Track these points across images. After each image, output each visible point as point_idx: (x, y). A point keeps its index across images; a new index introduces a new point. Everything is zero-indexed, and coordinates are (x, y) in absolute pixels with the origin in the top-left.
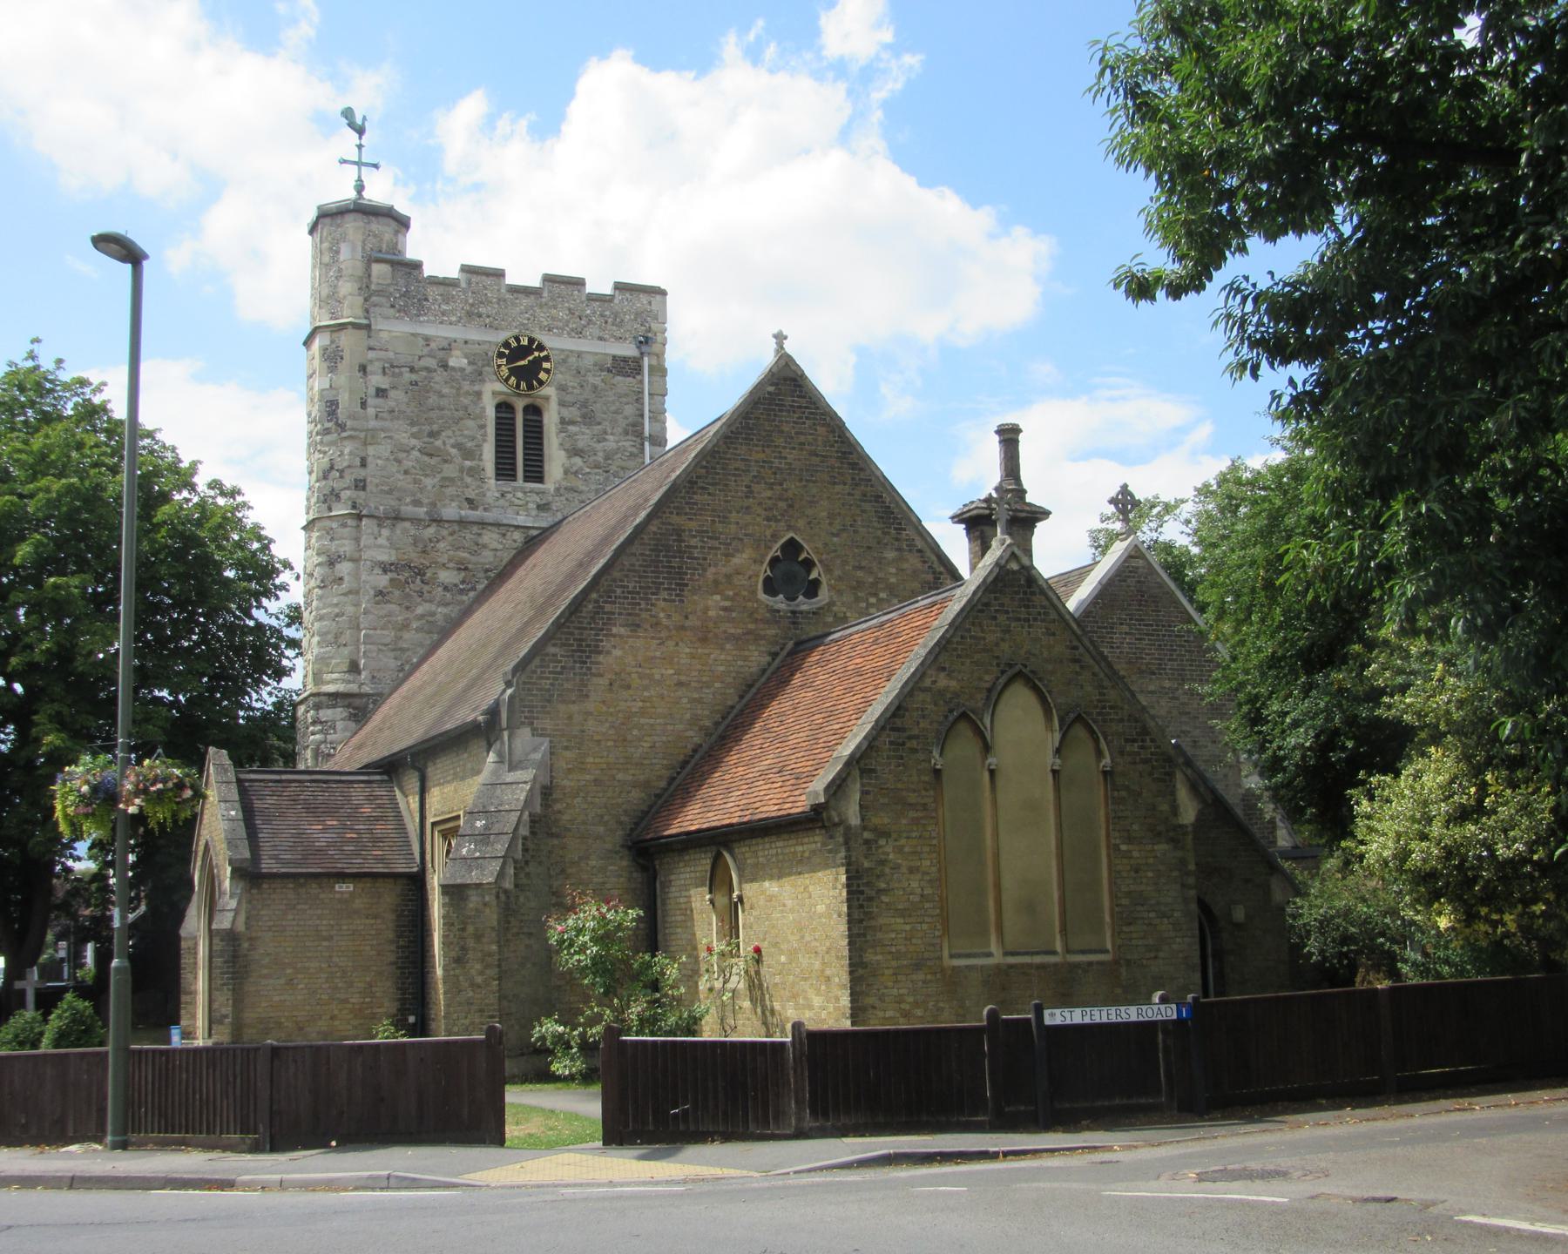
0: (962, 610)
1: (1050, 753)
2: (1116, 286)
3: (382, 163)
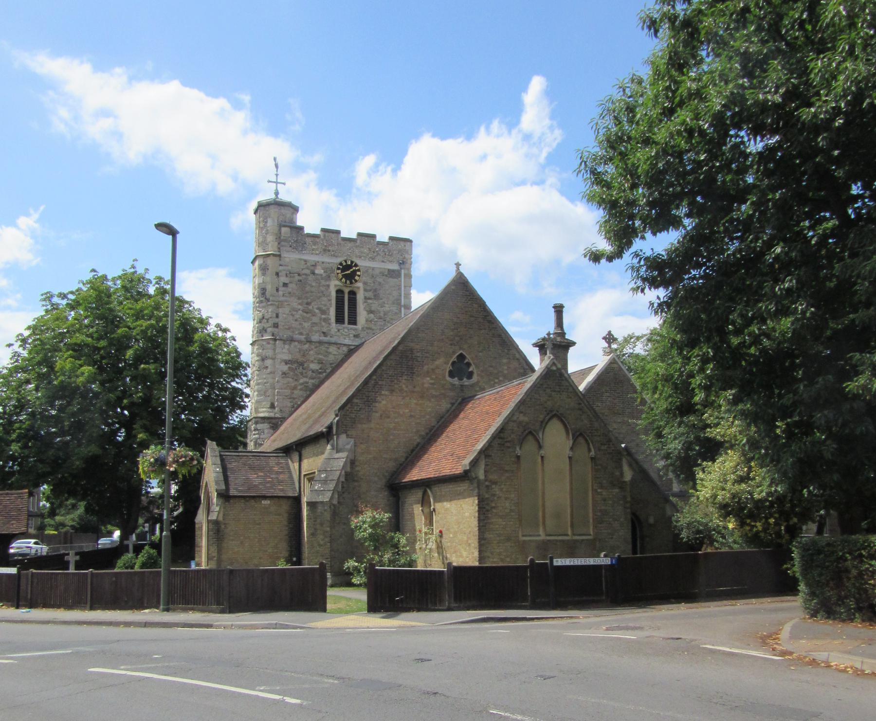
0: (531, 387)
1: (568, 449)
2: (585, 256)
3: (287, 183)
